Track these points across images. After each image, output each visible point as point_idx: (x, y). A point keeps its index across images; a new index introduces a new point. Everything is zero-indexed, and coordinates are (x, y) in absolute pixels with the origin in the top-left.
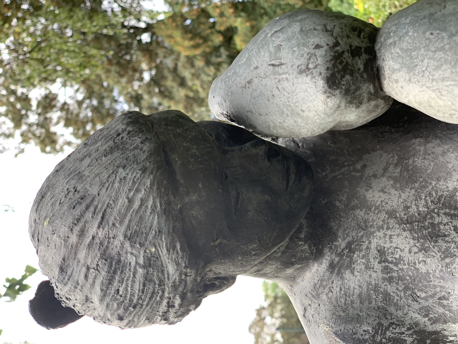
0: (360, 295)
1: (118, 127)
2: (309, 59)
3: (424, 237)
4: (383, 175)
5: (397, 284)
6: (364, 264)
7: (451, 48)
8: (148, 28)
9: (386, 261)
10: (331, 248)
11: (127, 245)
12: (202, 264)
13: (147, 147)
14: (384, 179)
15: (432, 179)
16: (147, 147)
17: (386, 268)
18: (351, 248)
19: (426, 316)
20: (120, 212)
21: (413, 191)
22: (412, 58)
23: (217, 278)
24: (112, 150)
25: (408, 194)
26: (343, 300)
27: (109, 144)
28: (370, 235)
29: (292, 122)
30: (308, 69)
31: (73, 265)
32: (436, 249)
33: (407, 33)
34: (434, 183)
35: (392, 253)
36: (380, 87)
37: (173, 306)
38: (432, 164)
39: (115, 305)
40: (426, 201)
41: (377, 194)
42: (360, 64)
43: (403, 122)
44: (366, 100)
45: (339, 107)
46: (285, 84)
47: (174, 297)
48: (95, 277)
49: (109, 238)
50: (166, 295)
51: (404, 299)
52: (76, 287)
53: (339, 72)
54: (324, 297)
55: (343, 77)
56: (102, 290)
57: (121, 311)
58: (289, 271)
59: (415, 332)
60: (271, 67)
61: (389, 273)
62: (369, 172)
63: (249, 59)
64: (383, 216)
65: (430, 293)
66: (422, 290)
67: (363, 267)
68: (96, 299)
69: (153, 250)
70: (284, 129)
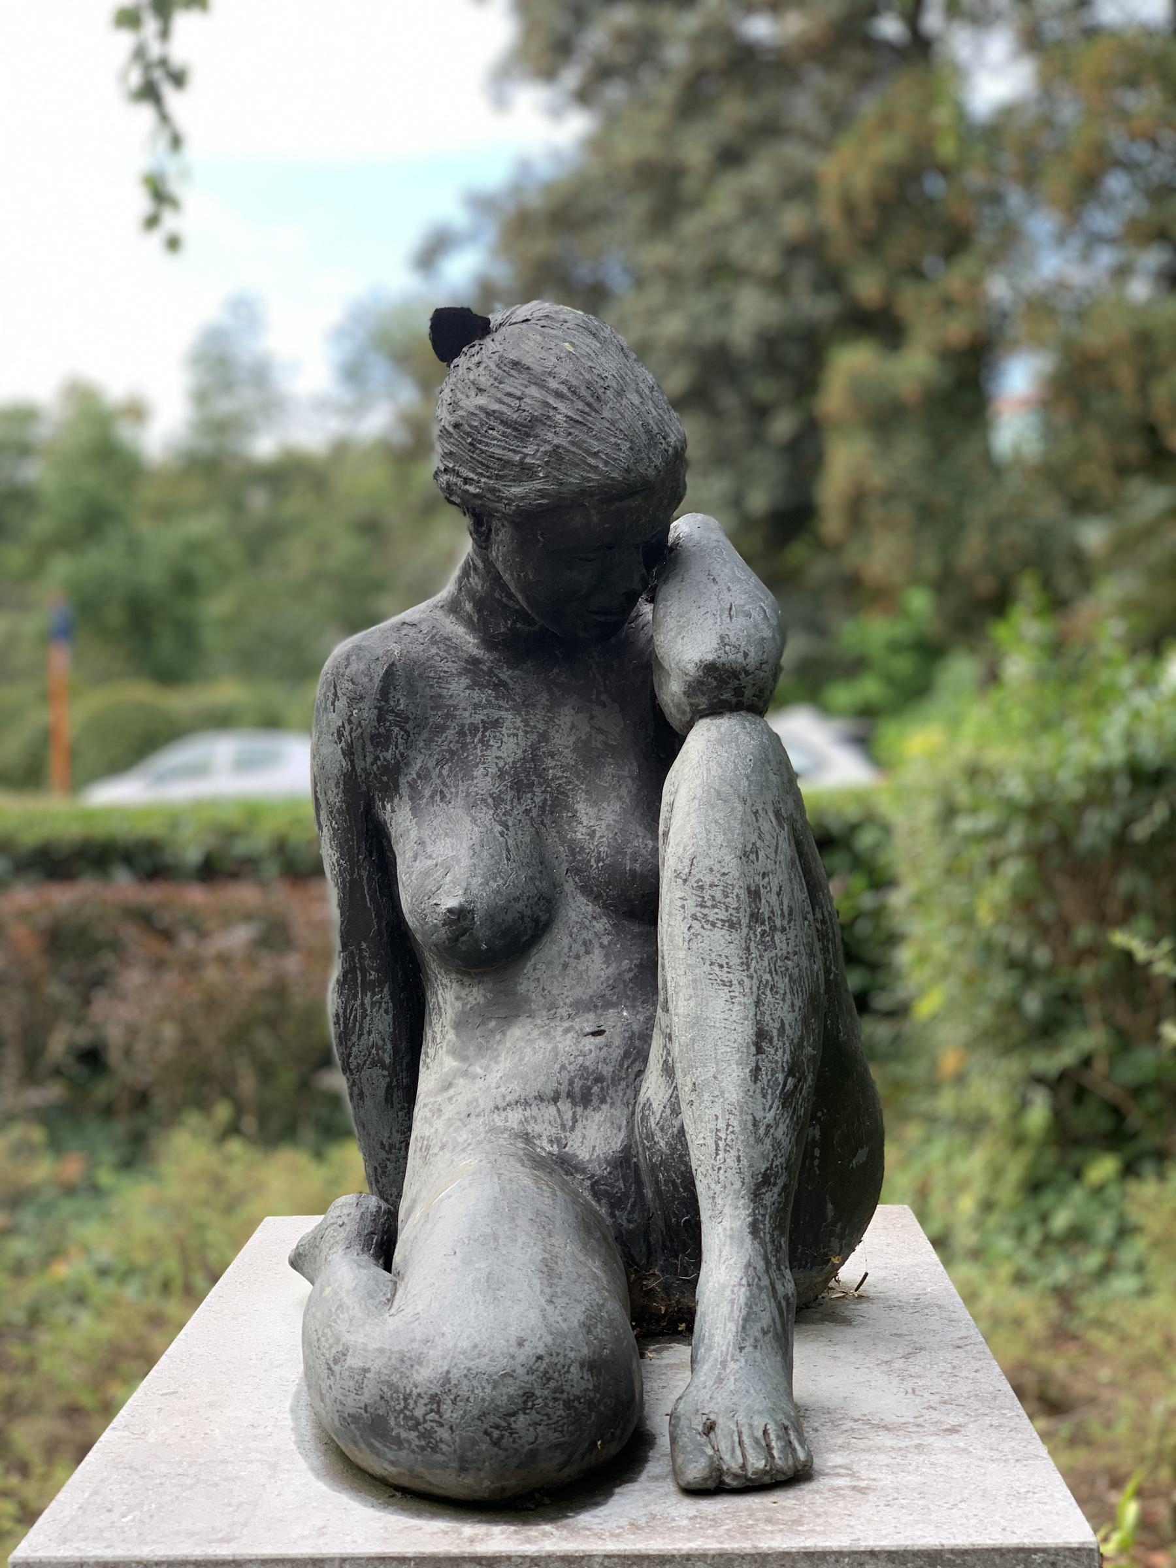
0: (440, 696)
3: (516, 774)
4: (592, 727)
5: (457, 742)
7: (736, 775)
8: (920, 47)
9: (486, 729)
10: (499, 661)
11: (548, 448)
12: (517, 520)
13: (651, 472)
16: (651, 472)
17: (477, 729)
19: (419, 776)
20: (584, 442)
22: (729, 742)
23: (490, 530)
24: (648, 432)
25: (570, 757)
26: (432, 674)
27: (655, 427)
28: (517, 710)
29: (672, 626)
31: (523, 378)
36: (704, 715)
37: (466, 483)
38: (607, 785)
39: (476, 424)
41: (568, 720)
42: (727, 696)
43: (660, 745)
45: (686, 675)
47: (480, 488)
50: (483, 480)
52: (496, 379)
53: (720, 675)
54: (434, 651)
55: (715, 679)
56: (494, 411)
58: (468, 606)
62: (597, 711)
63: (739, 580)
64: (541, 727)
66: (451, 770)
67: (476, 701)
68: (482, 400)
69: (541, 475)
70: (664, 616)
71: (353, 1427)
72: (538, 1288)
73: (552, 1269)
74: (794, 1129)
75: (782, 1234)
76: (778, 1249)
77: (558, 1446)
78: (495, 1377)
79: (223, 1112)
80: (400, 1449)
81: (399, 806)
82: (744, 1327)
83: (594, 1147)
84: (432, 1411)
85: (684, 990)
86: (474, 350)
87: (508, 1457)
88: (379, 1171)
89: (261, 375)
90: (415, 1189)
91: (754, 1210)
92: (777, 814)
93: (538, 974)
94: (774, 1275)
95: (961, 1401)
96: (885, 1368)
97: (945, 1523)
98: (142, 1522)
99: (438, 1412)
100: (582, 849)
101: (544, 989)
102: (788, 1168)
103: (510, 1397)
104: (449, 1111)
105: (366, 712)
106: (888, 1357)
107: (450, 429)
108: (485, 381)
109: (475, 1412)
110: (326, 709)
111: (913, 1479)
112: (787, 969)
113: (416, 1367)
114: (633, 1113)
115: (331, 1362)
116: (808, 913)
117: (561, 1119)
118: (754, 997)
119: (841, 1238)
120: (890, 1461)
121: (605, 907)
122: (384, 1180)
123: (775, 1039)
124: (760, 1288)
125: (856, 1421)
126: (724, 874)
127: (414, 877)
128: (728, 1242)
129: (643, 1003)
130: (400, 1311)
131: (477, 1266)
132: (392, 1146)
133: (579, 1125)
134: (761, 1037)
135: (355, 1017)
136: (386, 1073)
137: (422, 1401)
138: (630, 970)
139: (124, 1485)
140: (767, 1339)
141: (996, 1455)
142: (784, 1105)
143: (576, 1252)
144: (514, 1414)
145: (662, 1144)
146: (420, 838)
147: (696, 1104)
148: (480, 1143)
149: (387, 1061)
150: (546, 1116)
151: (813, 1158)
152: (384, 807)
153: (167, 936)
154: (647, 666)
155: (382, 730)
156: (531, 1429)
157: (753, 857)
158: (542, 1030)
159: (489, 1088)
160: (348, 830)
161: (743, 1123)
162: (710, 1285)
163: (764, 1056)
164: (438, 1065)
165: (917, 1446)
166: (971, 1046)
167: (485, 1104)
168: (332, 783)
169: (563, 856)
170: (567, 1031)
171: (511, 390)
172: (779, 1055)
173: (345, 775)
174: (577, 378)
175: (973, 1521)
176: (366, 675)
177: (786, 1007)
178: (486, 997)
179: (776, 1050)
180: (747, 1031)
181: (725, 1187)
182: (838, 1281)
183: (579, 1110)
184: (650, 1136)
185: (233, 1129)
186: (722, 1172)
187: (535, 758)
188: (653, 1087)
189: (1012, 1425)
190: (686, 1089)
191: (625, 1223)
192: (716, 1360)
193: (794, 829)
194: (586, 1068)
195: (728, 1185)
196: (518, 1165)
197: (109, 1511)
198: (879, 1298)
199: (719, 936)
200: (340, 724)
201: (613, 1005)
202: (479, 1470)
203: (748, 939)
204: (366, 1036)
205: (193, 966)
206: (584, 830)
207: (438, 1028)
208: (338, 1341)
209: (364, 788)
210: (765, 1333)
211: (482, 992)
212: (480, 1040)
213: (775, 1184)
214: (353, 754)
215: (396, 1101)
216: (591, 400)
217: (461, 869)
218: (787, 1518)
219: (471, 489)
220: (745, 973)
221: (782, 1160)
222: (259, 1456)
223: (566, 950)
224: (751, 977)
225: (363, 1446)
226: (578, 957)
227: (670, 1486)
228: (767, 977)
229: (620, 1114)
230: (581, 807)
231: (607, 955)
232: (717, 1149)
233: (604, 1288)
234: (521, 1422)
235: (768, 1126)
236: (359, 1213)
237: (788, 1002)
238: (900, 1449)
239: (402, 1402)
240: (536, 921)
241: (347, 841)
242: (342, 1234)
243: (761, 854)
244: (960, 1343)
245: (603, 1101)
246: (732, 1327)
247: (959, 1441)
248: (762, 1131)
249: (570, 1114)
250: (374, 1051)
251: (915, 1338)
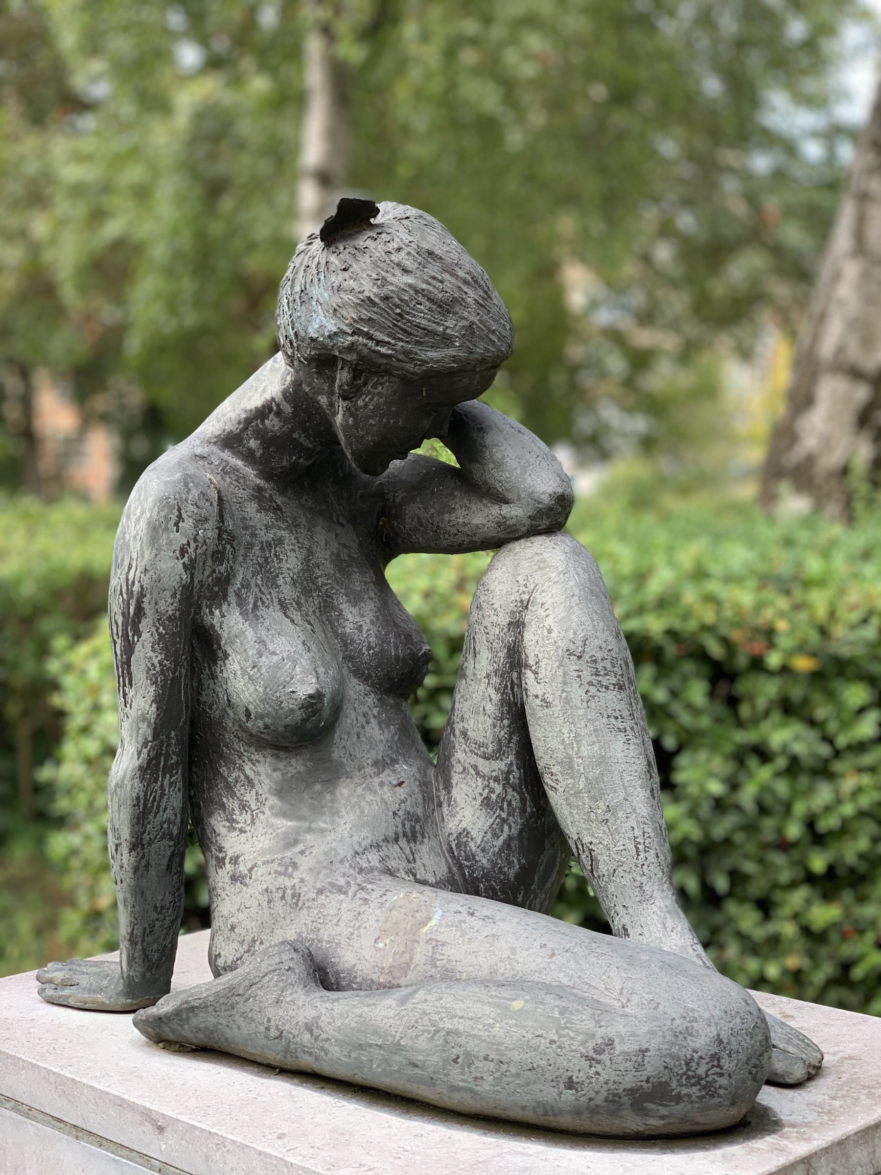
4: (339, 543)
11: (466, 323)
14: (336, 545)
15: (345, 589)
18: (277, 509)
25: (330, 568)
37: (377, 345)
40: (327, 584)
45: (539, 503)
50: (400, 344)
56: (423, 290)
59: (229, 575)
62: (339, 529)
68: (410, 280)
81: (228, 612)
84: (713, 1066)
85: (586, 739)
88: (147, 931)
93: (344, 743)
99: (719, 1066)
100: (353, 641)
101: (351, 755)
108: (409, 264)
109: (744, 1059)
121: (373, 685)
126: (610, 651)
135: (155, 797)
136: (172, 843)
137: (704, 1062)
145: (484, 861)
146: (259, 638)
147: (611, 821)
152: (212, 613)
155: (220, 548)
167: (344, 851)
173: (183, 587)
178: (305, 766)
181: (651, 877)
186: (645, 867)
199: (612, 695)
200: (185, 542)
206: (351, 626)
211: (301, 761)
212: (310, 801)
214: (194, 568)
219: (383, 350)
223: (355, 722)
230: (345, 607)
231: (379, 723)
245: (423, 837)
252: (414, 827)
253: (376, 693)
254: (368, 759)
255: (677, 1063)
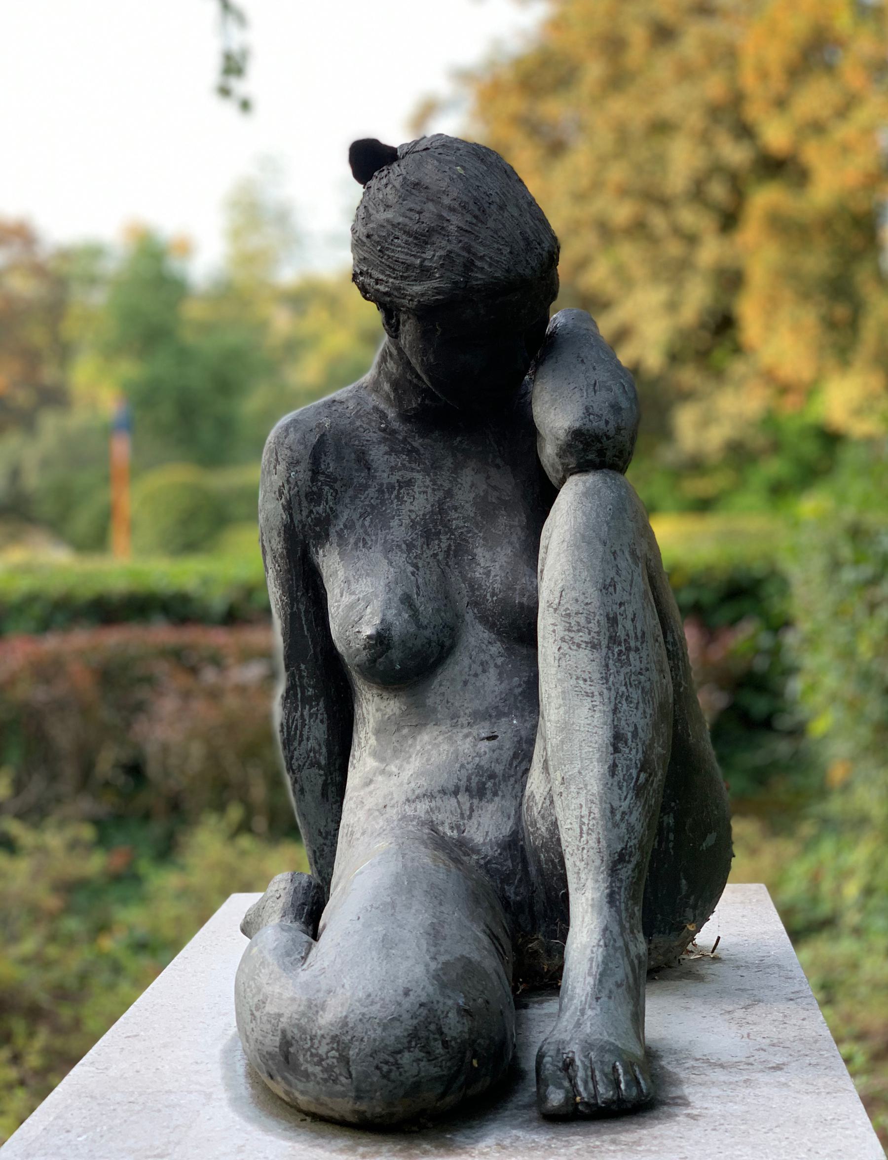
1: (546, 242)
2: (597, 416)
3: (425, 525)
4: (489, 485)
5: (377, 498)
6: (396, 465)
9: (401, 487)
13: (528, 272)
14: (485, 487)
16: (528, 272)
17: (393, 488)
18: (412, 452)
19: (345, 526)
21: (472, 515)
24: (526, 239)
25: (470, 510)
26: (357, 443)
27: (532, 235)
29: (547, 399)
30: (589, 415)
32: (415, 536)
33: (613, 492)
34: (481, 534)
35: (408, 494)
37: (377, 284)
38: (500, 533)
41: (469, 479)
42: (591, 456)
43: (541, 497)
44: (563, 461)
46: (578, 395)
47: (388, 287)
48: (411, 219)
49: (448, 236)
50: (391, 280)
51: (361, 504)
54: (358, 423)
56: (399, 224)
57: (375, 238)
58: (386, 387)
60: (593, 382)
61: (388, 490)
62: (493, 471)
64: (447, 485)
65: (369, 530)
66: (371, 522)
67: (393, 464)
68: (389, 215)
69: (437, 275)
70: (541, 391)
71: (270, 1062)
72: (425, 947)
73: (438, 932)
74: (646, 816)
75: (636, 904)
76: (632, 916)
77: (440, 1078)
78: (385, 1021)
79: (235, 813)
80: (308, 1081)
82: (600, 981)
83: (487, 832)
84: (333, 1049)
86: (384, 174)
87: (395, 1088)
89: (282, 217)
90: (341, 867)
91: (611, 883)
92: (633, 553)
94: (628, 937)
95: (787, 1044)
96: (727, 1017)
97: (760, 1145)
98: (94, 1141)
100: (480, 586)
101: (448, 702)
102: (641, 847)
103: (397, 1038)
104: (370, 803)
105: (303, 474)
106: (731, 1008)
107: (364, 239)
109: (368, 1050)
110: (269, 472)
111: (737, 1108)
112: (640, 683)
113: (321, 1013)
114: (521, 804)
115: (253, 1009)
116: (659, 636)
117: (461, 809)
118: (612, 706)
119: (695, 907)
120: (721, 1093)
121: (499, 633)
122: (321, 861)
123: (630, 740)
124: (616, 949)
125: (697, 1060)
126: (587, 604)
127: (340, 610)
128: (590, 910)
129: (530, 712)
130: (310, 966)
131: (375, 929)
132: (327, 833)
133: (475, 814)
134: (617, 740)
135: (296, 726)
136: (322, 772)
138: (520, 685)
139: (84, 1111)
140: (620, 991)
141: (811, 1088)
142: (637, 796)
143: (463, 917)
144: (400, 1052)
145: (543, 829)
148: (393, 829)
149: (323, 762)
150: (448, 807)
151: (668, 841)
152: (317, 552)
153: (194, 671)
154: (529, 432)
155: (315, 489)
156: (415, 1064)
157: (611, 589)
158: (446, 735)
159: (401, 784)
160: (289, 571)
161: (602, 811)
162: (574, 946)
163: (620, 755)
164: (362, 764)
165: (745, 1081)
166: (854, 760)
168: (275, 533)
169: (464, 592)
170: (466, 736)
171: (412, 206)
172: (633, 754)
174: (467, 195)
175: (784, 1143)
176: (301, 444)
177: (639, 714)
179: (631, 750)
180: (603, 735)
182: (695, 945)
183: (475, 801)
184: (534, 823)
185: (245, 827)
186: (585, 851)
187: (441, 511)
188: (536, 783)
189: (827, 1064)
190: (557, 783)
191: (512, 896)
192: (576, 1008)
193: (648, 567)
194: (481, 767)
195: (590, 862)
196: (422, 848)
197: (68, 1131)
198: (730, 960)
201: (505, 715)
202: (372, 1098)
203: (607, 657)
204: (305, 742)
205: (214, 695)
207: (362, 735)
208: (259, 990)
209: (301, 537)
210: (619, 986)
212: (395, 744)
213: (629, 862)
215: (330, 795)
216: (477, 213)
217: (377, 605)
218: (629, 1140)
220: (605, 686)
221: (636, 841)
222: (198, 1087)
223: (467, 669)
224: (609, 689)
225: (279, 1079)
226: (476, 675)
227: (534, 1113)
228: (623, 689)
229: (509, 805)
230: (479, 551)
231: (500, 674)
232: (581, 833)
233: (485, 948)
234: (406, 1058)
235: (624, 813)
236: (293, 888)
237: (641, 710)
238: (731, 1083)
239: (309, 1042)
240: (442, 646)
241: (287, 580)
242: (280, 903)
243: (619, 587)
244: (792, 996)
245: (495, 794)
246: (590, 980)
247: (780, 1076)
248: (618, 817)
249: (468, 805)
250: (312, 754)
251: (755, 992)
252: (484, 784)
253: (502, 642)
254: (467, 708)
255: (303, 1036)
